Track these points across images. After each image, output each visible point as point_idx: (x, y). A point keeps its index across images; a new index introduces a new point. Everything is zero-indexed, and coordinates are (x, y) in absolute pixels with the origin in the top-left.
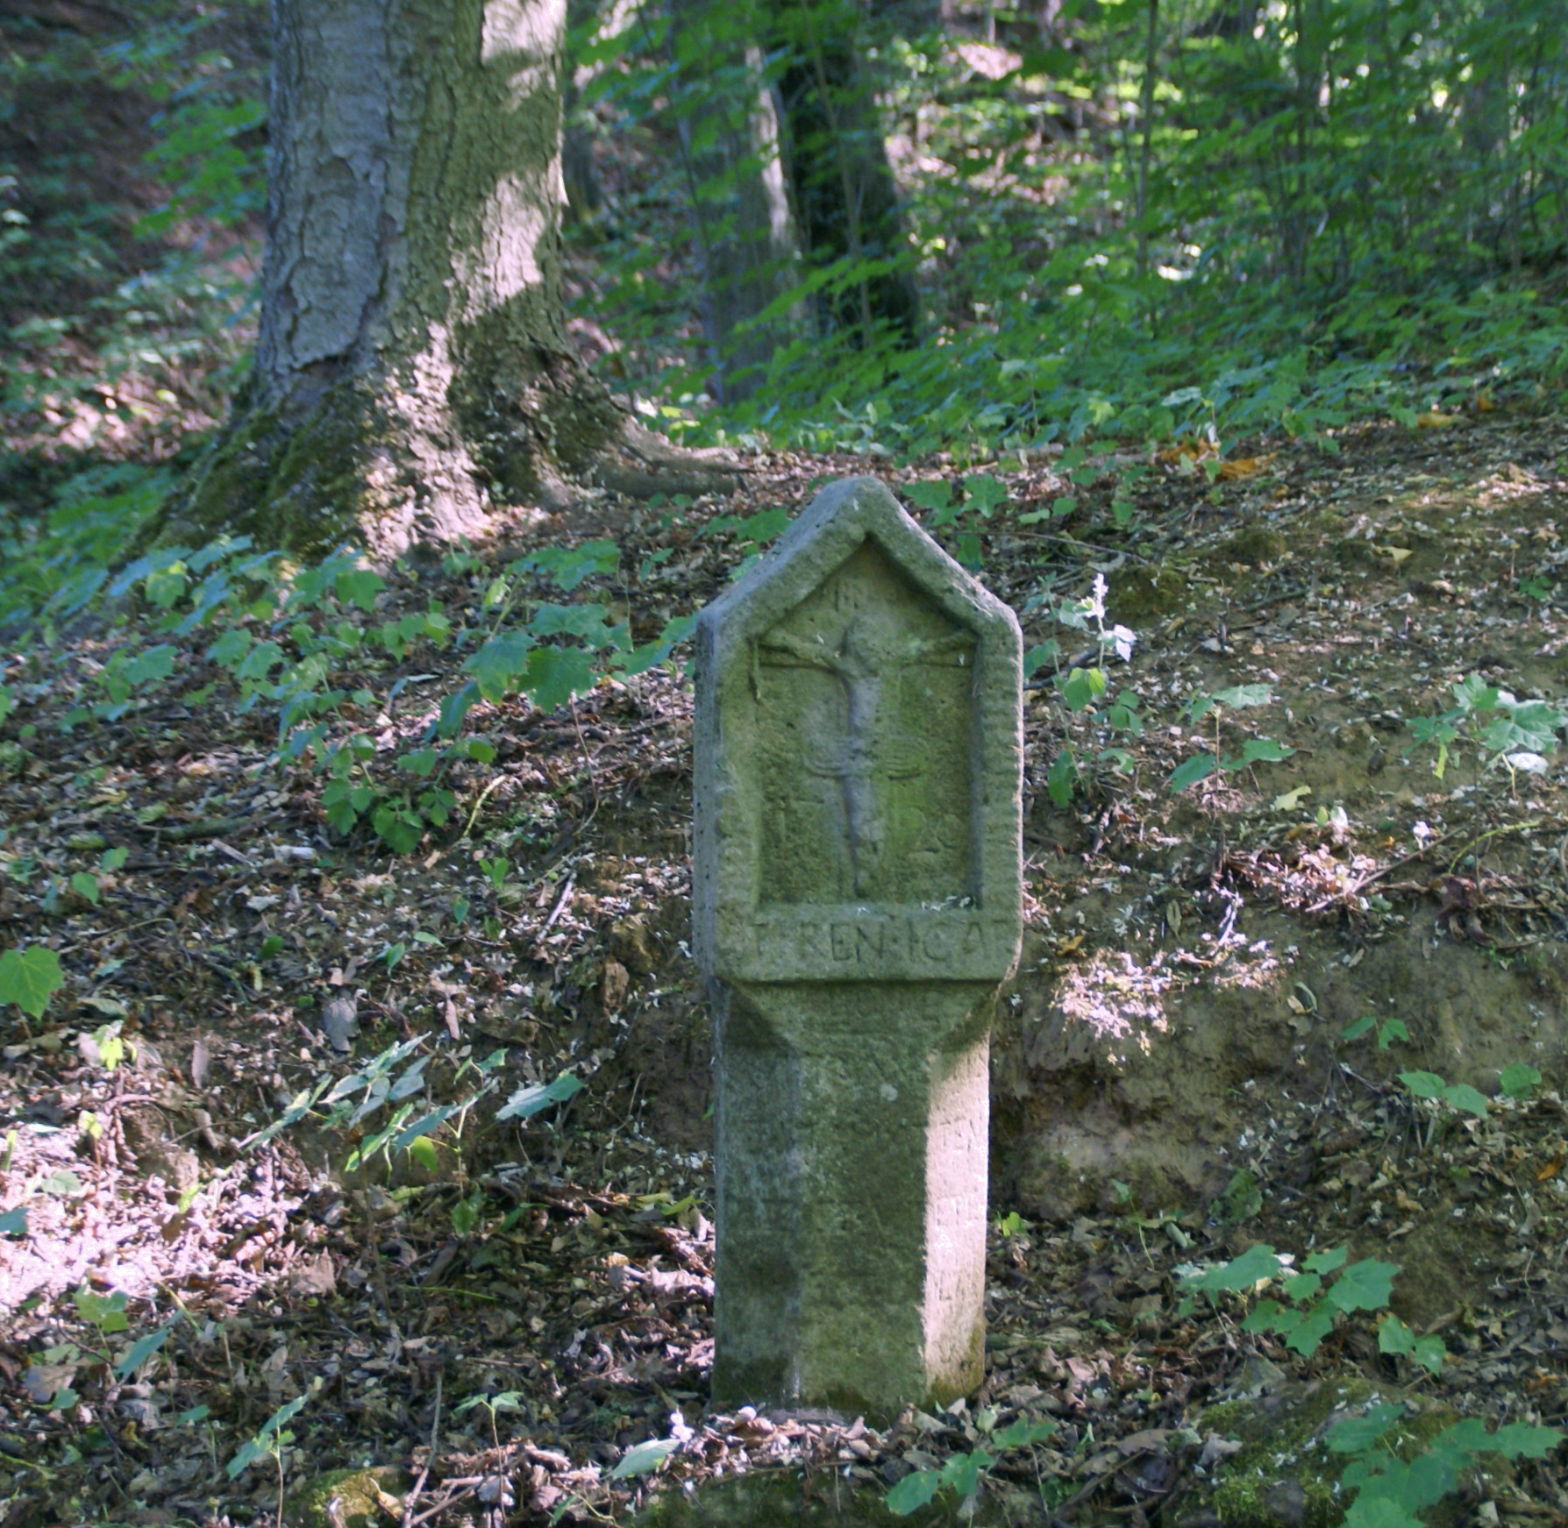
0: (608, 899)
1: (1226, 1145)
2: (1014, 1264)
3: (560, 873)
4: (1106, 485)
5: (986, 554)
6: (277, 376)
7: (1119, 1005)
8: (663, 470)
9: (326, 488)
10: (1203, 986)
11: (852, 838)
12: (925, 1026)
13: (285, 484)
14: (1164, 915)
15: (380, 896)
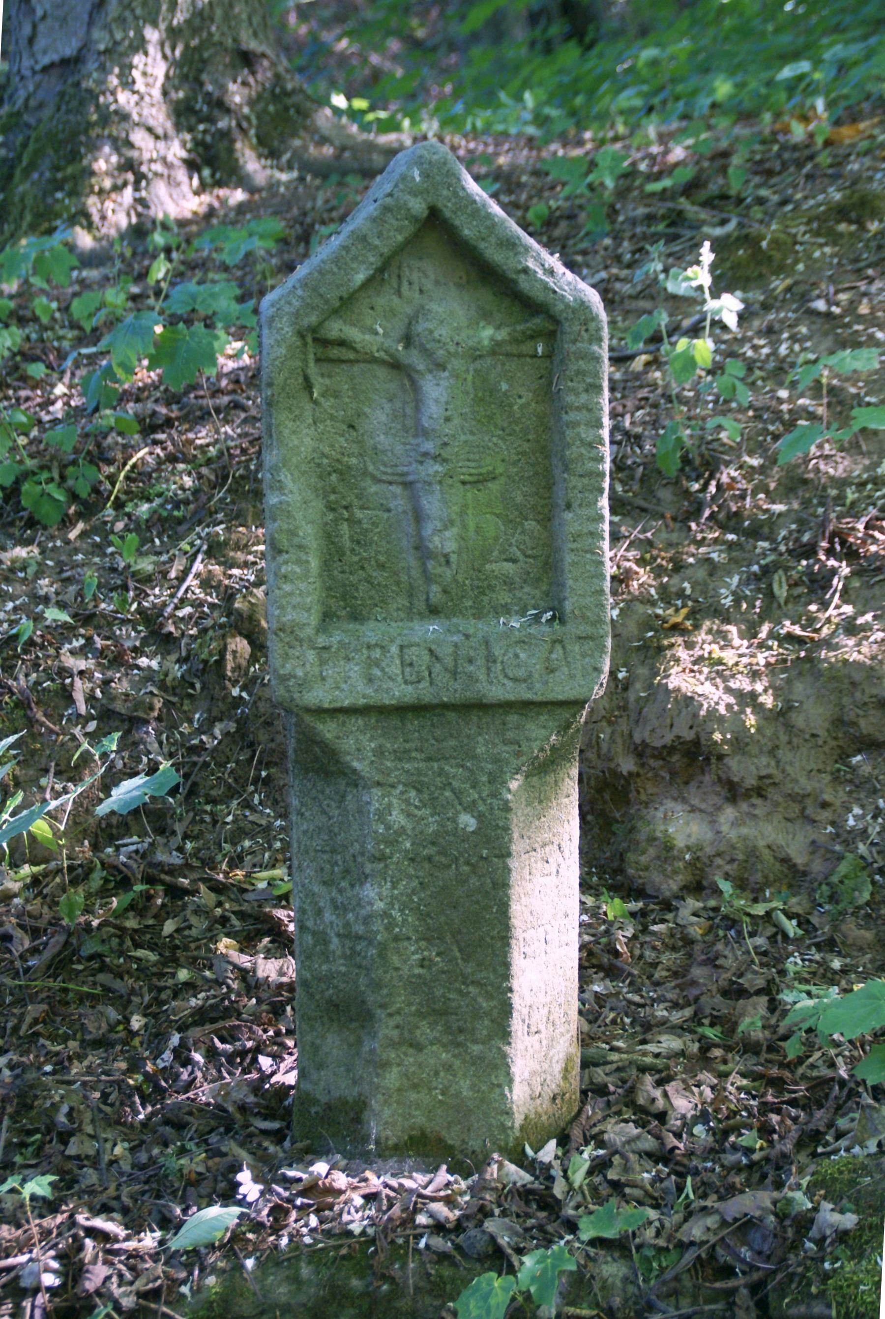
0: (235, 572)
1: (833, 823)
2: (617, 954)
3: (192, 544)
4: (725, 155)
5: (613, 222)
6: (22, 78)
7: (725, 680)
8: (347, 154)
9: (60, 175)
10: (809, 659)
11: (421, 549)
12: (505, 751)
13: (27, 172)
14: (770, 586)
15: (24, 569)
